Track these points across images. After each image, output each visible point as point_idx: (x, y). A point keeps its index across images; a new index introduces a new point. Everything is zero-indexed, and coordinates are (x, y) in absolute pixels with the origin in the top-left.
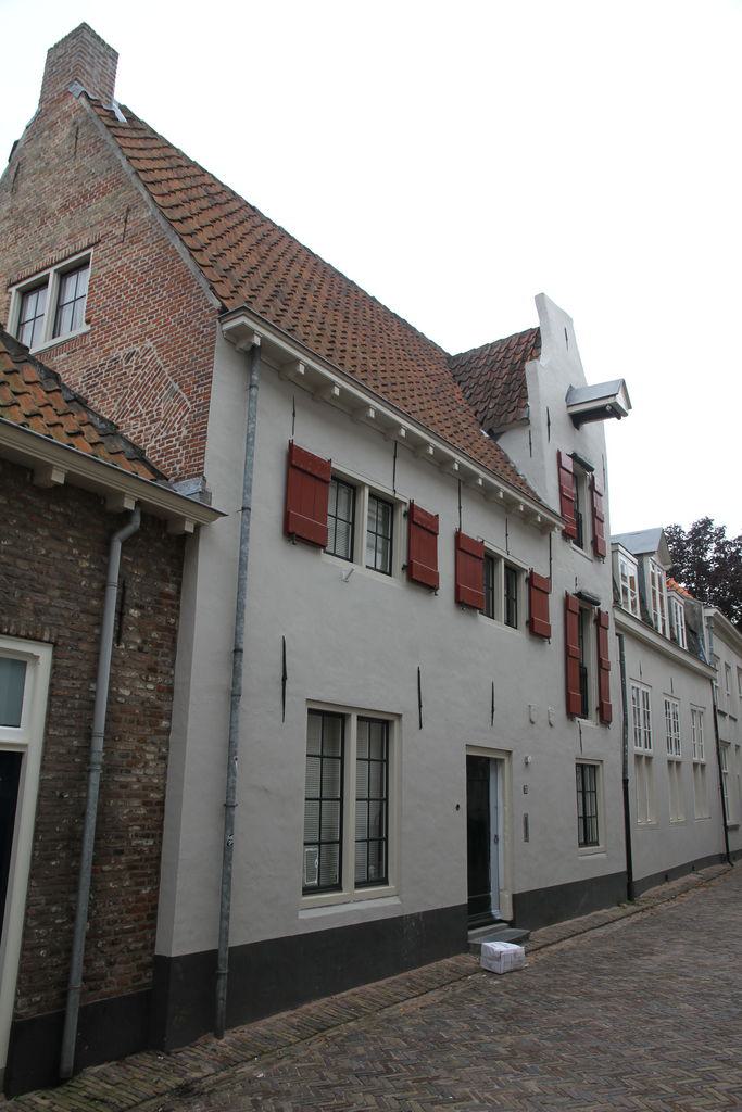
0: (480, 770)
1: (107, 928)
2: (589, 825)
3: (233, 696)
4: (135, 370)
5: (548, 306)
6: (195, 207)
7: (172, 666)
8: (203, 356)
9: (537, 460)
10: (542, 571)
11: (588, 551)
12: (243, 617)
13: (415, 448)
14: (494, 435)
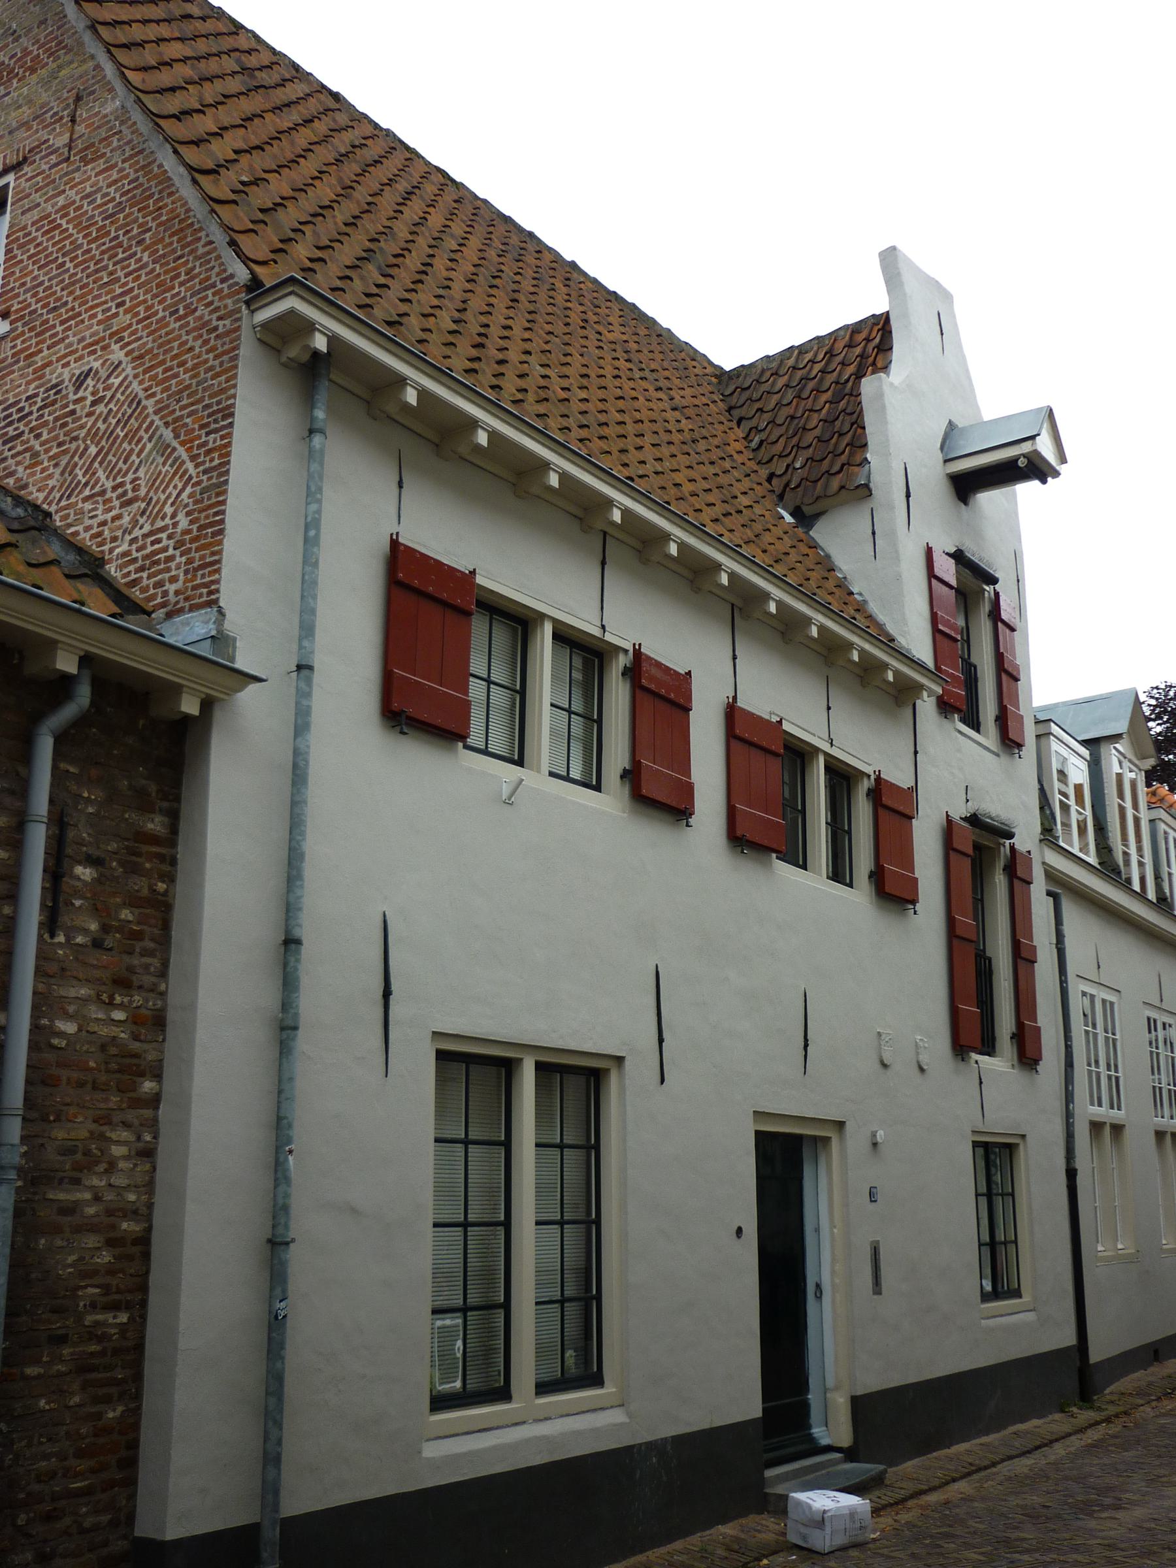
0: (784, 1160)
1: (36, 1487)
2: (1001, 1257)
3: (282, 1029)
4: (94, 403)
5: (901, 265)
6: (210, 92)
7: (163, 973)
8: (218, 375)
9: (888, 562)
10: (900, 777)
11: (990, 736)
12: (299, 877)
13: (643, 544)
14: (805, 519)
